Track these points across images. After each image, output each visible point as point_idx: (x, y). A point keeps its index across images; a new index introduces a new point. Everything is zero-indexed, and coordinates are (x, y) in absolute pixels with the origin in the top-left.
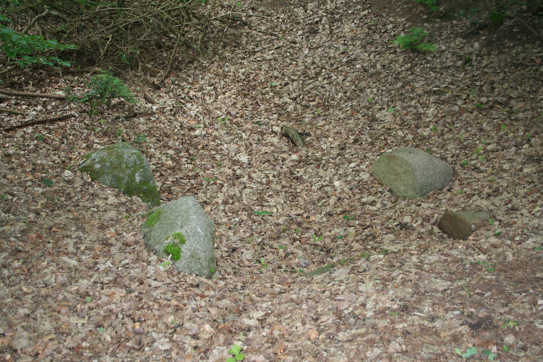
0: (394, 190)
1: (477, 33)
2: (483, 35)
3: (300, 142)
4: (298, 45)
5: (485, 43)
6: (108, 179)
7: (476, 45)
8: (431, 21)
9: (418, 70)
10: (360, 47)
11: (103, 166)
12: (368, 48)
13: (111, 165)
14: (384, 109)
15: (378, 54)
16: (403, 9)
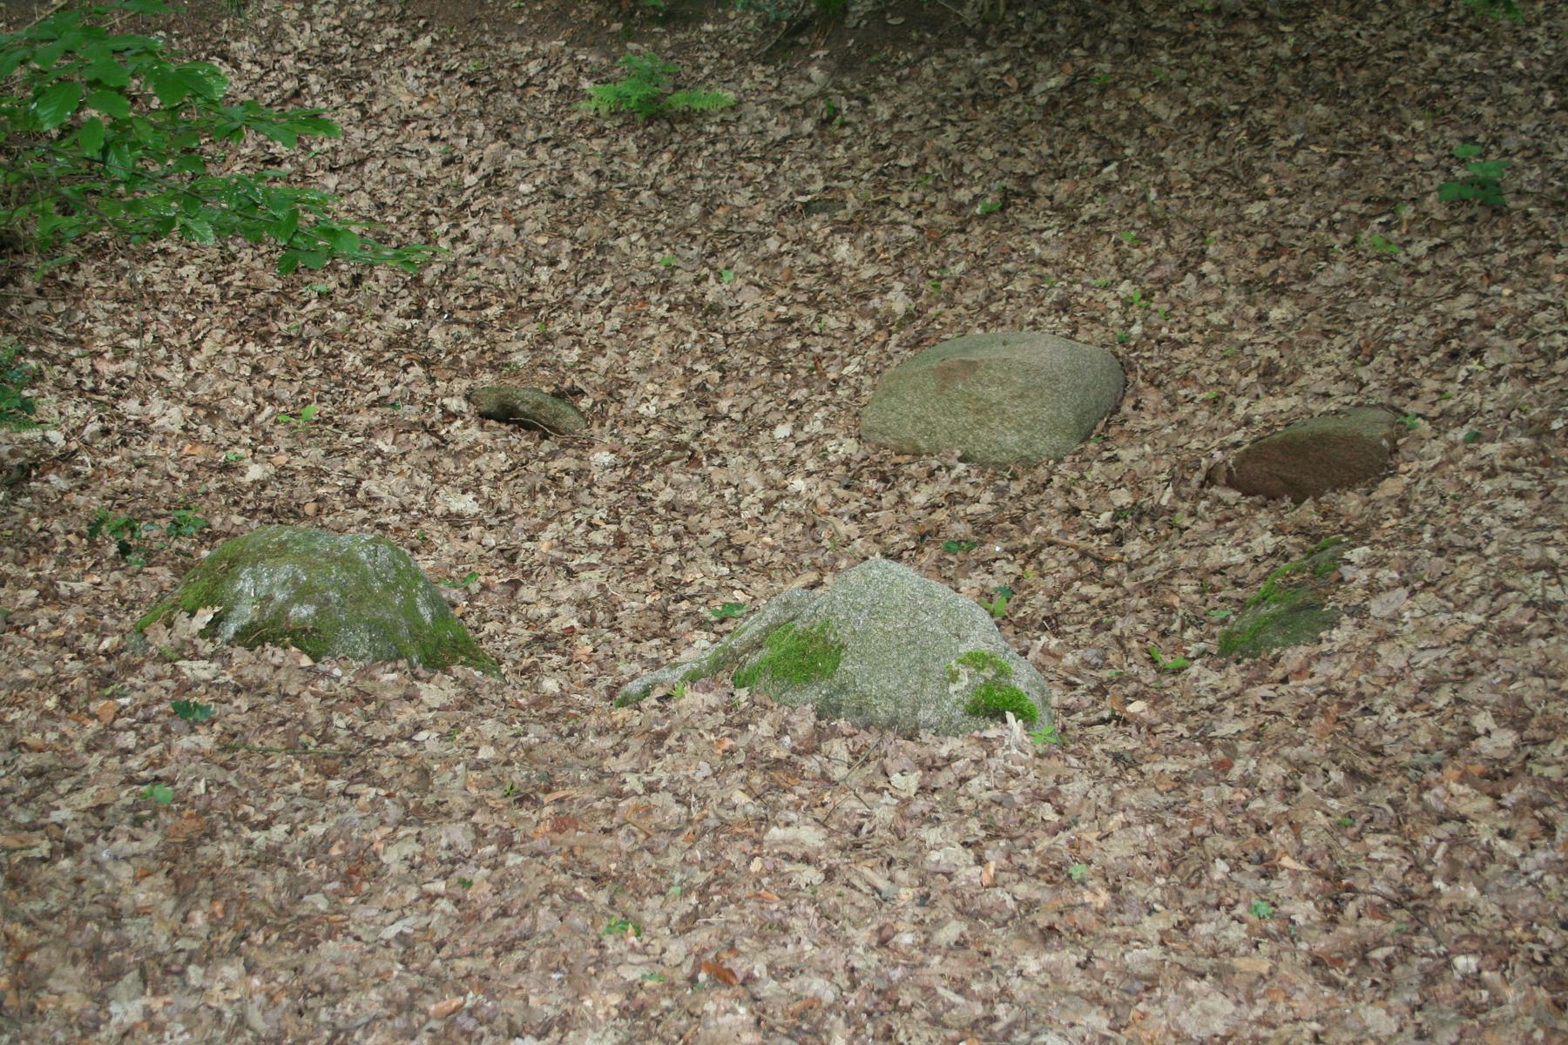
0: (978, 451)
1: (794, 44)
2: (814, 47)
3: (570, 419)
4: (287, 167)
5: (832, 64)
6: (360, 639)
7: (815, 72)
8: (640, 34)
9: (700, 165)
10: (490, 138)
11: (323, 606)
12: (516, 136)
13: (344, 595)
14: (706, 278)
15: (557, 146)
16: (535, 16)
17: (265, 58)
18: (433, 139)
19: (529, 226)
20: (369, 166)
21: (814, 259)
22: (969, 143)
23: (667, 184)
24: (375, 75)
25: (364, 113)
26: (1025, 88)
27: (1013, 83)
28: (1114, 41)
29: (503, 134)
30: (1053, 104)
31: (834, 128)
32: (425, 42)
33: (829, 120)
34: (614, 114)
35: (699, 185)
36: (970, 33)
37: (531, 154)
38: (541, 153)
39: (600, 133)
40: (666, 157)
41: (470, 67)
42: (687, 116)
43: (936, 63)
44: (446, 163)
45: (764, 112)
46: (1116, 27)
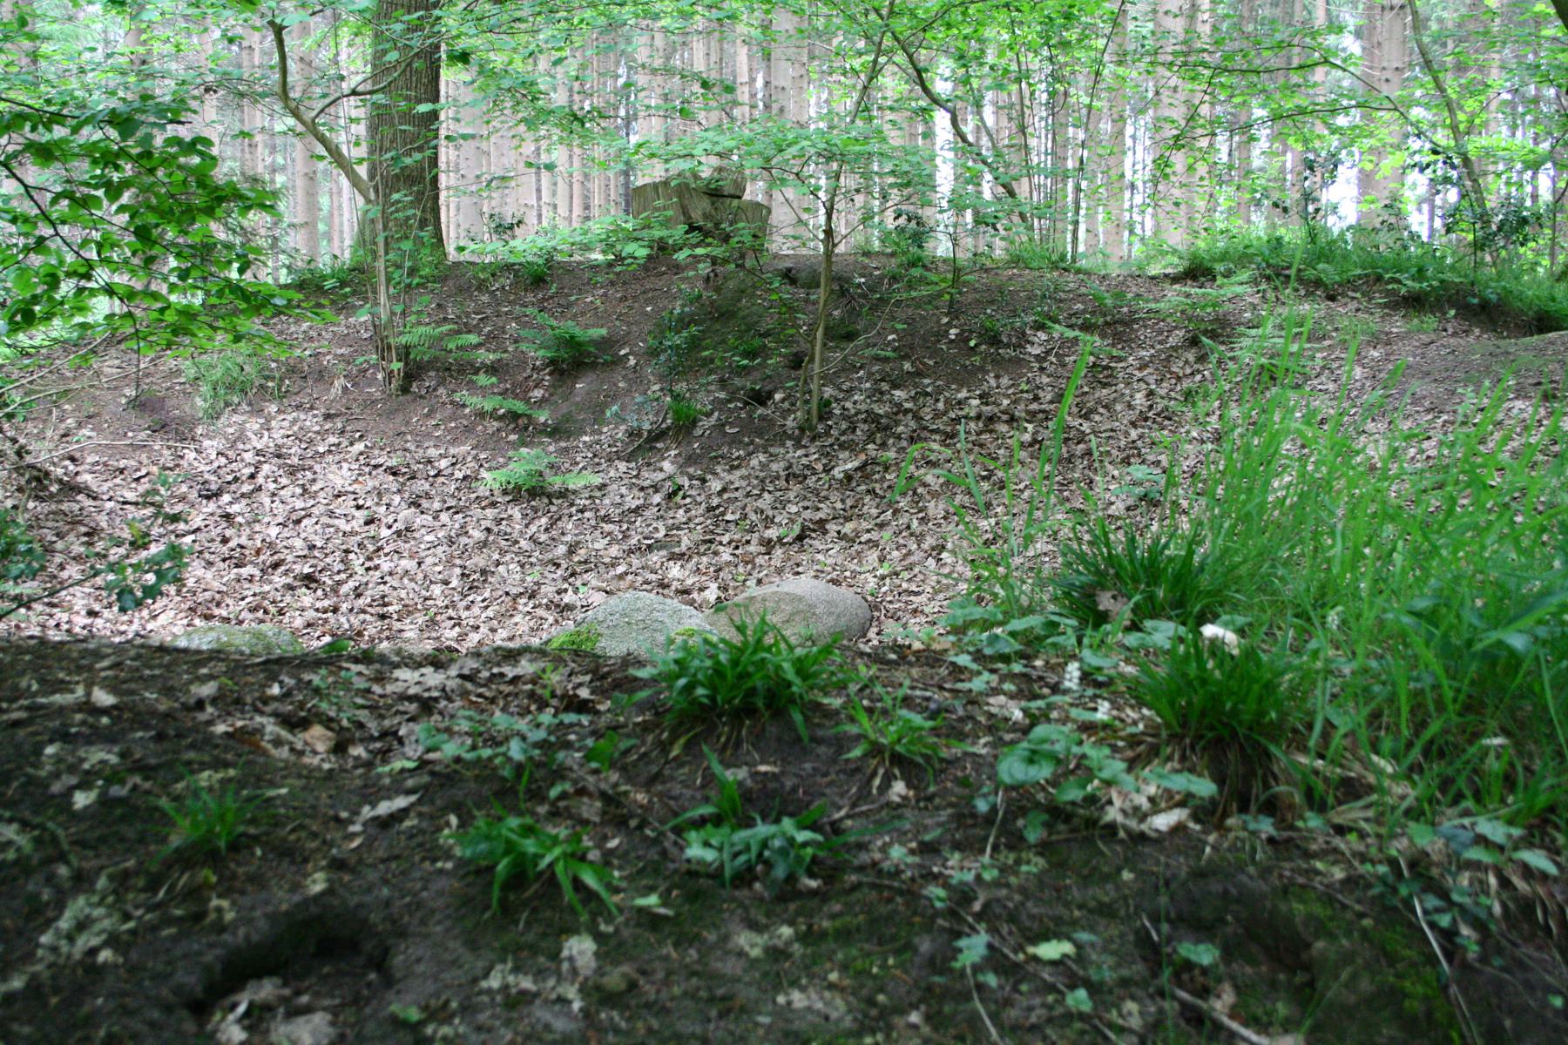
17: (231, 454)
18: (359, 507)
19: (429, 561)
20: (305, 522)
21: (653, 577)
22: (781, 504)
23: (543, 537)
24: (317, 468)
25: (305, 490)
26: (827, 470)
27: (819, 467)
28: (899, 438)
29: (415, 504)
30: (849, 478)
31: (678, 499)
32: (360, 447)
33: (675, 493)
34: (505, 492)
35: (568, 538)
36: (790, 437)
37: (436, 518)
38: (444, 517)
39: (493, 505)
40: (544, 520)
41: (393, 462)
42: (564, 494)
43: (762, 457)
44: (367, 523)
45: (624, 490)
46: (901, 429)
